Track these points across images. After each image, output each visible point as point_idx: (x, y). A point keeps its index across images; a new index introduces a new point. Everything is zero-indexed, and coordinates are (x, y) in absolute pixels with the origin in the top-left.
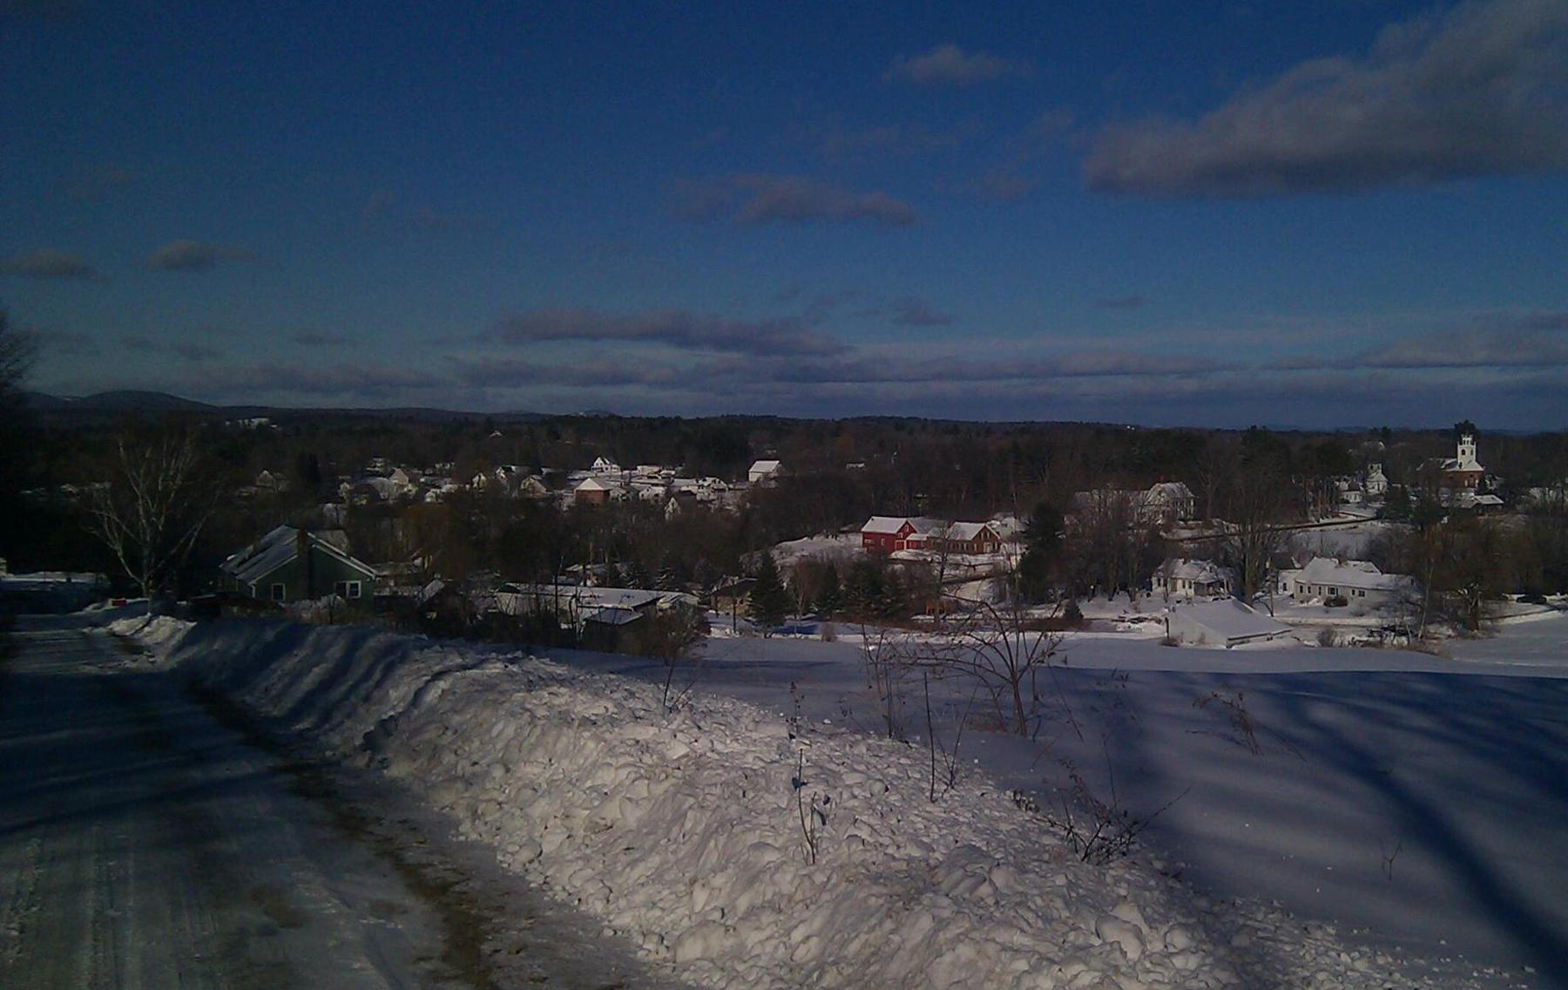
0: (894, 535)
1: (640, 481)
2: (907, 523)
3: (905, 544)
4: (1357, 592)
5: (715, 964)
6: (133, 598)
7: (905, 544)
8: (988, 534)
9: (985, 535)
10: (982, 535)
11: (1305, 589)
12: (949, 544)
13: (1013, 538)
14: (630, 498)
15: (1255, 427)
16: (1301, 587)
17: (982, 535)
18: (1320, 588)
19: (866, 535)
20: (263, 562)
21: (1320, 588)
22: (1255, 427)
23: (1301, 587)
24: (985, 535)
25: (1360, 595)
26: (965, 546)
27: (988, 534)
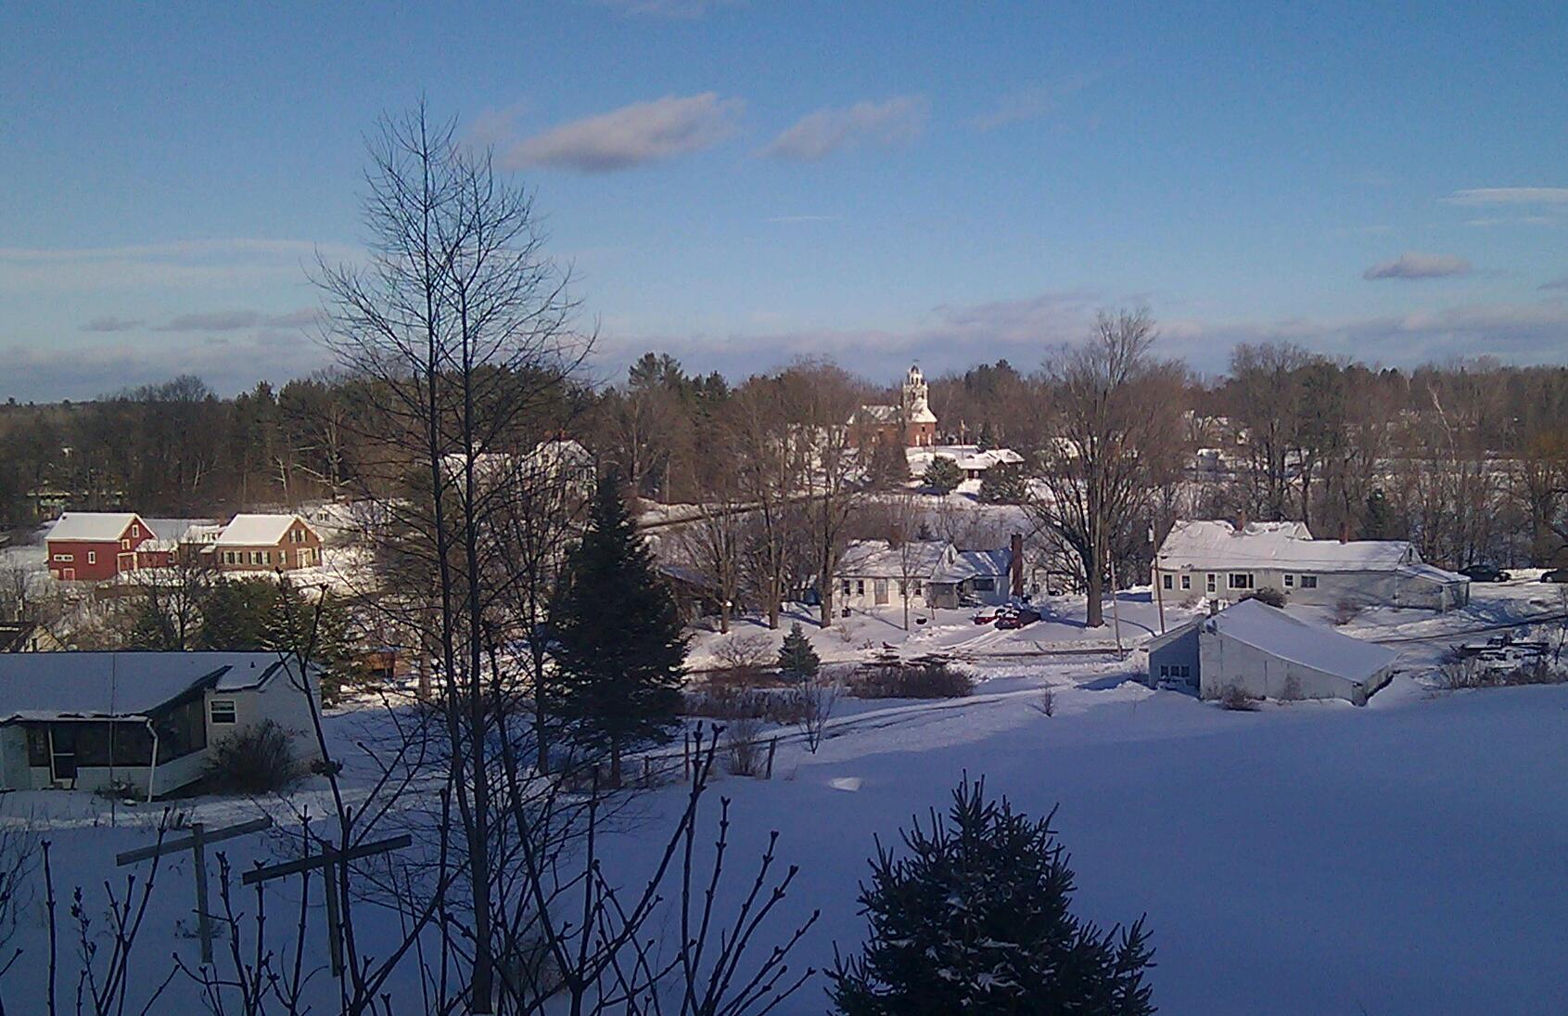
0: (115, 543)
1: (1099, 490)
2: (136, 521)
3: (135, 558)
4: (1297, 580)
5: (538, 942)
6: (1009, 943)
7: (135, 558)
8: (303, 533)
9: (298, 534)
10: (293, 534)
11: (1178, 582)
12: (259, 555)
13: (342, 542)
14: (740, 519)
15: (652, 355)
16: (1168, 578)
17: (293, 534)
18: (1211, 577)
19: (55, 547)
20: (30, 815)
21: (1211, 577)
22: (652, 355)
23: (1168, 578)
24: (298, 534)
25: (1304, 585)
26: (264, 555)
27: (303, 533)
